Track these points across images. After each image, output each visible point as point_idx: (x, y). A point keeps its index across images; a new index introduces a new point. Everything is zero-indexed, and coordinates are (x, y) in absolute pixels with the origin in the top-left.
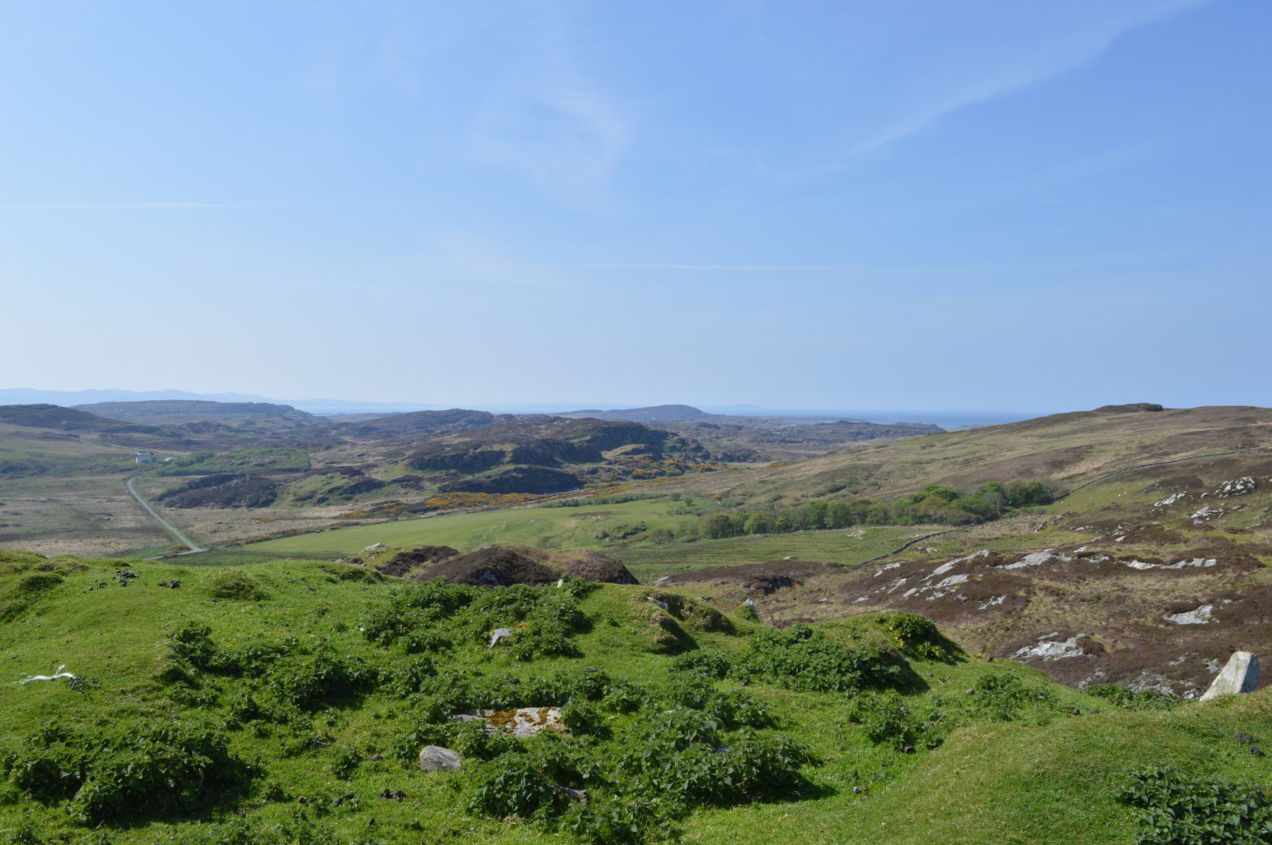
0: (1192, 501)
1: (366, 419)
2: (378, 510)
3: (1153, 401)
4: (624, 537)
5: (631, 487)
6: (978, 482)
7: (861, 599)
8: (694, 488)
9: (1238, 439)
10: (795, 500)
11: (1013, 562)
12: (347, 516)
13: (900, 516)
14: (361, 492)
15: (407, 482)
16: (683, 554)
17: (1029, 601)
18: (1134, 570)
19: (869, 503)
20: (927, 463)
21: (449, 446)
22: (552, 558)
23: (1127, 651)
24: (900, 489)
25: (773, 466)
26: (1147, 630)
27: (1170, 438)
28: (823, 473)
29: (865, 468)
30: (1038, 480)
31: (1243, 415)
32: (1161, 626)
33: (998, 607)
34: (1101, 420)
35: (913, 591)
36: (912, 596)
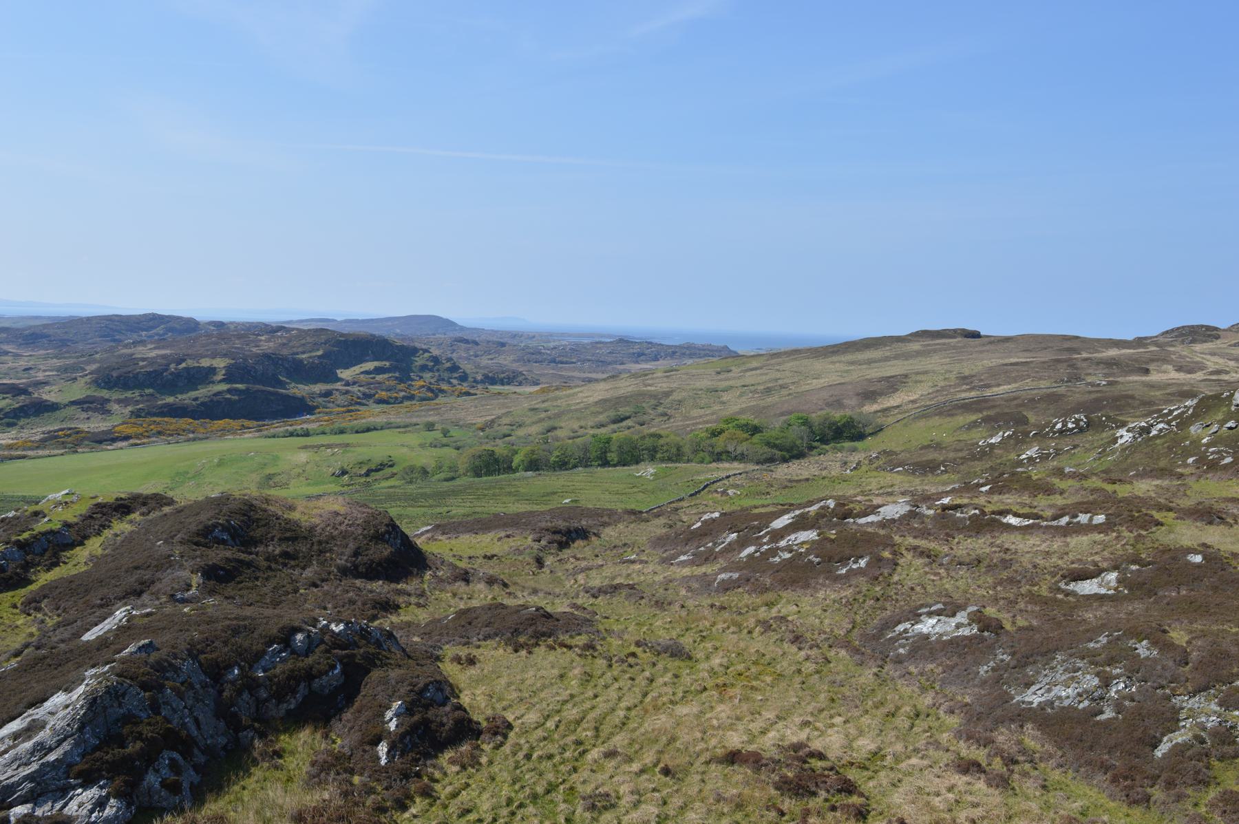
0: (1020, 440)
1: (32, 323)
2: (51, 439)
3: (970, 327)
4: (367, 474)
5: (373, 414)
6: (782, 414)
7: (683, 558)
8: (450, 415)
9: (1063, 371)
10: (575, 430)
11: (866, 515)
12: (10, 447)
13: (696, 452)
14: (27, 416)
15: (87, 405)
16: (441, 496)
17: (896, 564)
18: (1009, 527)
19: (660, 436)
20: (723, 391)
21: (143, 359)
22: (300, 509)
23: (1030, 628)
24: (692, 421)
25: (543, 391)
26: (1045, 602)
27: (991, 368)
28: (605, 401)
29: (653, 396)
30: (848, 413)
31: (1067, 345)
32: (1060, 596)
33: (860, 571)
34: (916, 346)
35: (751, 549)
36: (750, 556)
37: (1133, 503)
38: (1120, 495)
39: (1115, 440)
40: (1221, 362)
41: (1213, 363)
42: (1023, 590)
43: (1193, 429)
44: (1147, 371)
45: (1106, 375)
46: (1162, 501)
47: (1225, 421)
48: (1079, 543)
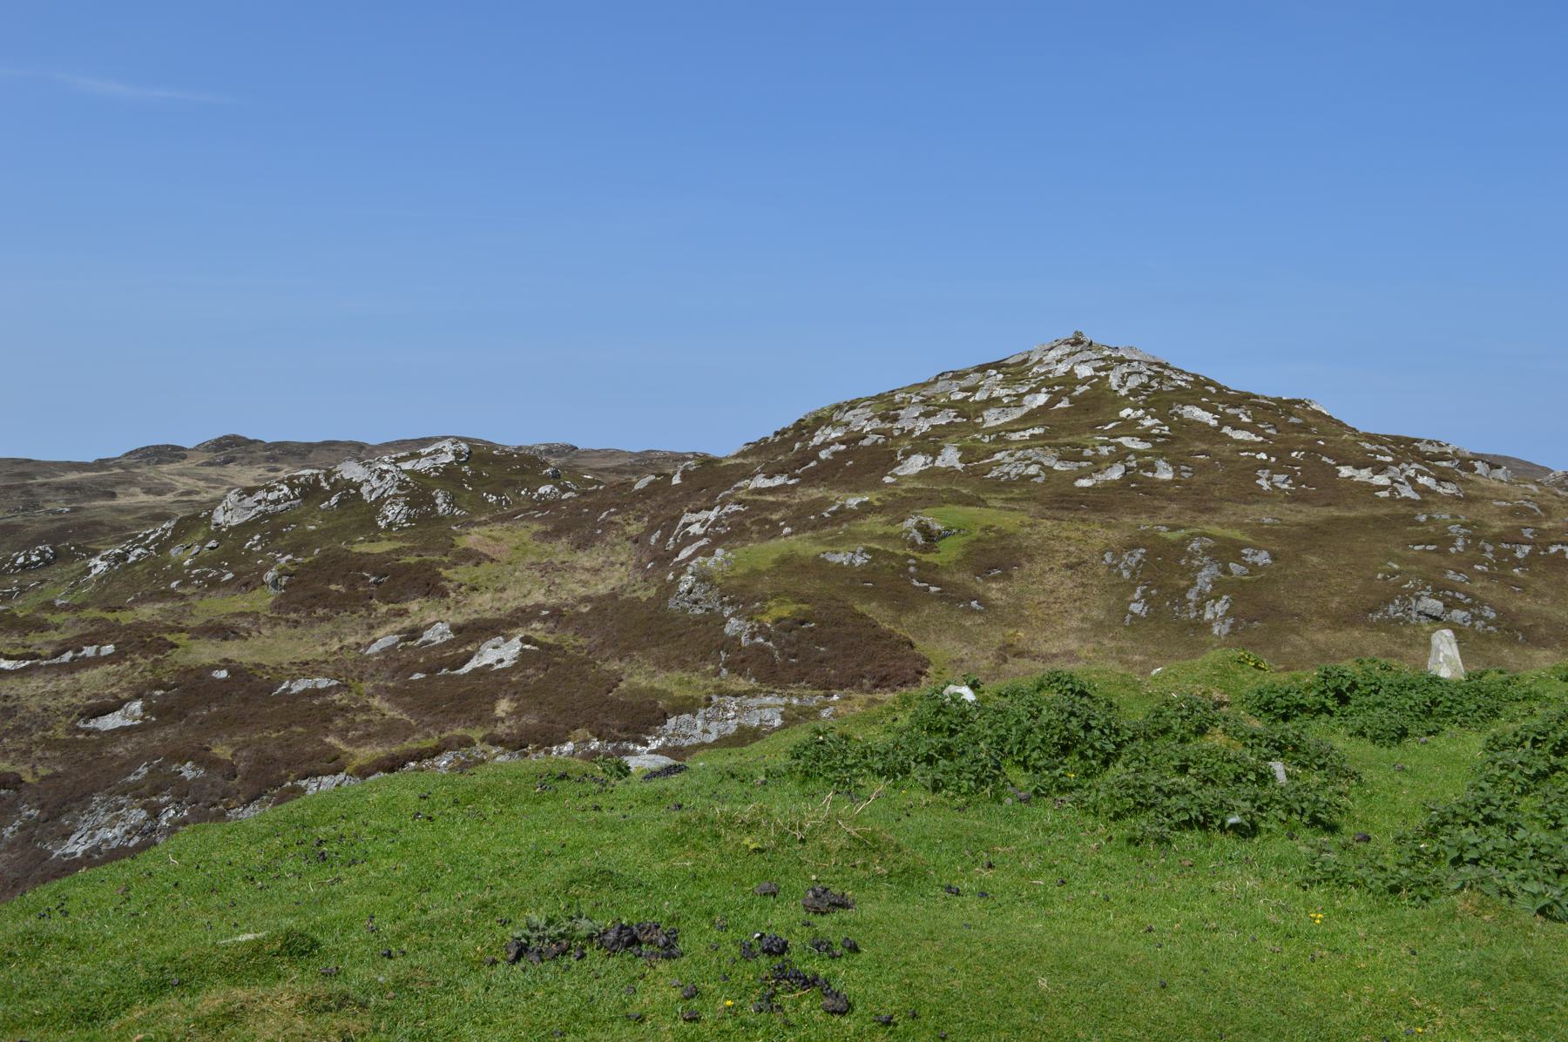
23: (56, 775)
26: (65, 745)
31: (17, 470)
32: (80, 737)
37: (138, 627)
38: (124, 623)
39: (88, 571)
40: (190, 483)
41: (182, 484)
42: (36, 737)
43: (173, 552)
44: (113, 495)
45: (68, 501)
46: (170, 623)
47: (203, 543)
48: (92, 680)
